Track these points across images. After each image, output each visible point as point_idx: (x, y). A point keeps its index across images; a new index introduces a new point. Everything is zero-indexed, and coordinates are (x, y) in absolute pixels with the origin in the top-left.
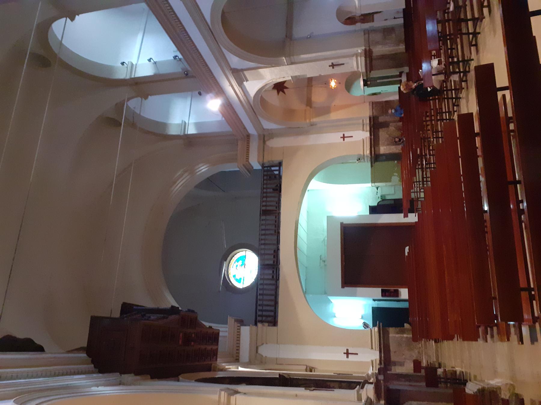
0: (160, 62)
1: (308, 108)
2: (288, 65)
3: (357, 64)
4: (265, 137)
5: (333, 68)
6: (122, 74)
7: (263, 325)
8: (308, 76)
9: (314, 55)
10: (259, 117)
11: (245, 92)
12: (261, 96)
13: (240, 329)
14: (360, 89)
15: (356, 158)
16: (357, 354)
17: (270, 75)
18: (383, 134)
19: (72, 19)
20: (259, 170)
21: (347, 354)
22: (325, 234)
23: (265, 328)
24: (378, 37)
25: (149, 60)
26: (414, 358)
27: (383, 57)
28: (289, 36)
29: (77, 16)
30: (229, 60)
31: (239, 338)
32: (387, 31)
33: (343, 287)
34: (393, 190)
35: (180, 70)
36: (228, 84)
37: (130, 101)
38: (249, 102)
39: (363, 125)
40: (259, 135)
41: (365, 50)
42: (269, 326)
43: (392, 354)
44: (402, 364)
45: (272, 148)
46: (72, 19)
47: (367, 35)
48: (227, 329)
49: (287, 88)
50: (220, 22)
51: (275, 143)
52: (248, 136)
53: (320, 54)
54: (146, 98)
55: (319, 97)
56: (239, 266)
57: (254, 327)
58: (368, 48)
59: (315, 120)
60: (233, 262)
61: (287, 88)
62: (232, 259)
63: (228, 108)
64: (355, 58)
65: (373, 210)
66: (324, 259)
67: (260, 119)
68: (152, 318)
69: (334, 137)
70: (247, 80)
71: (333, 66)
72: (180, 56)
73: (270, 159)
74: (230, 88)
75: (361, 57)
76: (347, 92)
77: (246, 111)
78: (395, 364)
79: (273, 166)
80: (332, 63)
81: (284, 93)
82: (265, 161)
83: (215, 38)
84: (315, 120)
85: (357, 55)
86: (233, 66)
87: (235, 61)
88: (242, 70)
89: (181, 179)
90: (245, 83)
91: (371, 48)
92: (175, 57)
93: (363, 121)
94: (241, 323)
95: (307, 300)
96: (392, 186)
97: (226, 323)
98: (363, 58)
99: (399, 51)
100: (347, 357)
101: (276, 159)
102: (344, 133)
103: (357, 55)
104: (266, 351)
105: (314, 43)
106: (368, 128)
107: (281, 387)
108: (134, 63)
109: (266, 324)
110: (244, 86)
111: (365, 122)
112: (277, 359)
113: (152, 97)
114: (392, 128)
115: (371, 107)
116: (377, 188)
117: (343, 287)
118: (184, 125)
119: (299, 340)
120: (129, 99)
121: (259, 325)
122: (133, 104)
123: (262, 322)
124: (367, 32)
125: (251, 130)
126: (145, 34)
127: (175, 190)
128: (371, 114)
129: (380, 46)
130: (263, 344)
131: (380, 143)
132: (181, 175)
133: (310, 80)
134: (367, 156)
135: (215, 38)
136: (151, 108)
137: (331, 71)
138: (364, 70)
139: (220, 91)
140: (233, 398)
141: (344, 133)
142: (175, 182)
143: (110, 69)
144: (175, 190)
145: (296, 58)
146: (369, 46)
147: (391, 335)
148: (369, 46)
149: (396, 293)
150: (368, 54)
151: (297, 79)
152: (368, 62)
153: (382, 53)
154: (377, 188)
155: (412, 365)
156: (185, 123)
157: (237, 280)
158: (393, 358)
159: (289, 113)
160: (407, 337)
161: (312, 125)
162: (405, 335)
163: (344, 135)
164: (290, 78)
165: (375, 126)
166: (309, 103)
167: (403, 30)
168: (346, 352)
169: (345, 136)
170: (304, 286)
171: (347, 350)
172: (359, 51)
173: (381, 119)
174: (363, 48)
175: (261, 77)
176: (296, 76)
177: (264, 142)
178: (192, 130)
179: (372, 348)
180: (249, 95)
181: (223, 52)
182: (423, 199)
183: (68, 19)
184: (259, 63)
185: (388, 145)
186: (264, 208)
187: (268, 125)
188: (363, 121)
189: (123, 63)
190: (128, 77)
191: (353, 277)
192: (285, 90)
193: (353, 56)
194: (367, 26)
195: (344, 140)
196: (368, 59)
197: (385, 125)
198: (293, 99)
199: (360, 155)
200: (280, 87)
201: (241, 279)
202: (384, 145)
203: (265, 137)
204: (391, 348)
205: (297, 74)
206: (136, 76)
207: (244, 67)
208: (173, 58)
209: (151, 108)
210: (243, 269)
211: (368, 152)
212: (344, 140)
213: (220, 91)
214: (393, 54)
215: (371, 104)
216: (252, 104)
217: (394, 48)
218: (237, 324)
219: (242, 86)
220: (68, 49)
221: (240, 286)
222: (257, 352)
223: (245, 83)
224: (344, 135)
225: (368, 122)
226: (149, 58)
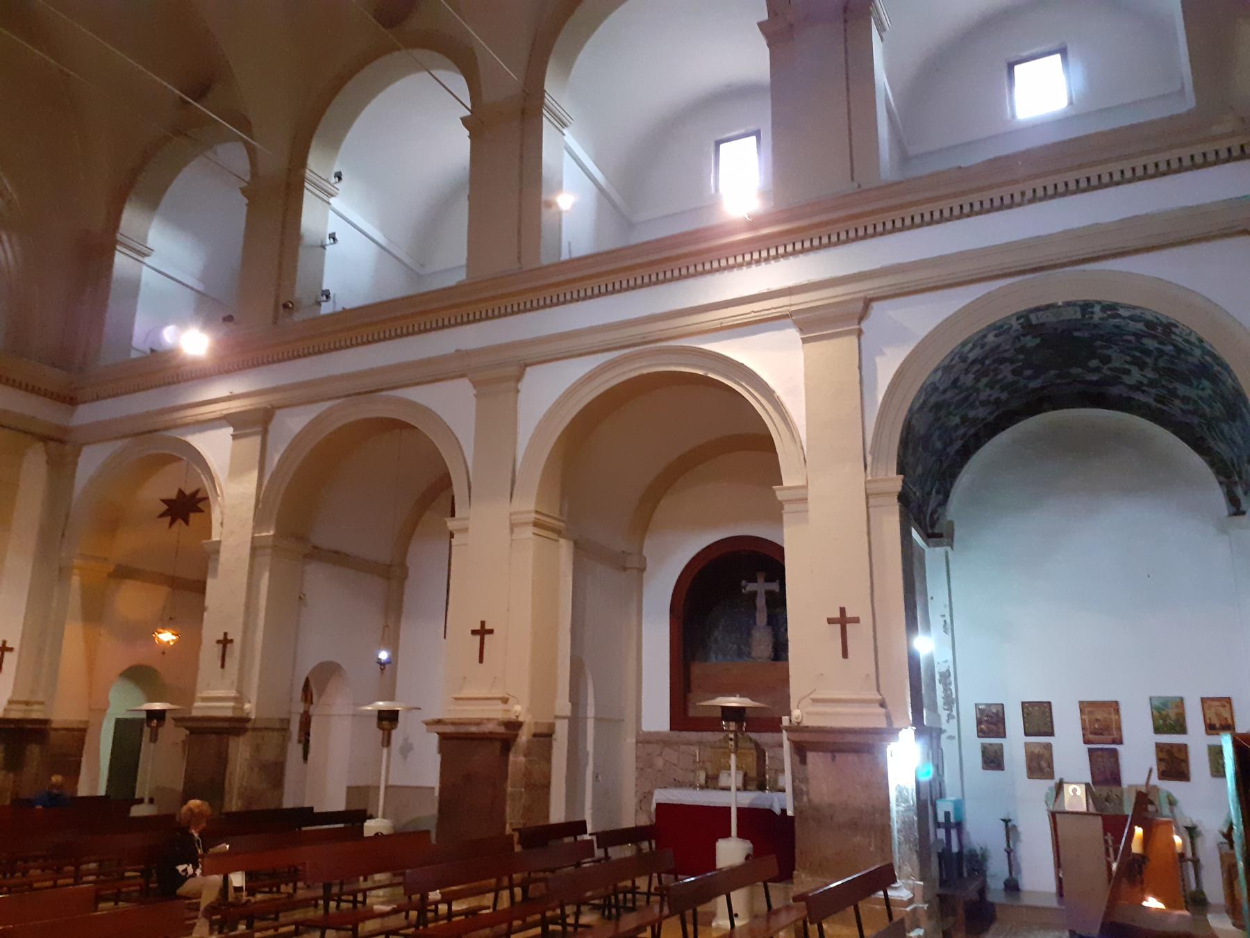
0: (323, 255)
1: (111, 568)
2: (253, 538)
3: (215, 695)
5: (218, 642)
6: (315, 164)
8: (210, 583)
9: (263, 602)
10: (126, 441)
12: (180, 459)
14: (126, 702)
24: (269, 755)
25: (333, 236)
27: (222, 760)
28: (316, 554)
32: (275, 773)
35: (298, 293)
37: (245, 152)
38: (176, 427)
39: (27, 703)
40: (66, 430)
41: (248, 720)
47: (278, 726)
49: (171, 523)
50: (395, 417)
52: (71, 400)
53: (262, 614)
55: (132, 601)
58: (249, 725)
59: (76, 580)
61: (171, 523)
63: (162, 370)
64: (233, 693)
67: (119, 444)
70: (235, 437)
71: (225, 642)
72: (326, 308)
74: (228, 393)
75: (234, 708)
76: (125, 667)
77: (149, 415)
80: (231, 641)
83: (359, 394)
84: (76, 580)
85: (239, 699)
86: (278, 413)
87: (293, 423)
88: (264, 434)
91: (249, 734)
92: (327, 294)
93: (42, 703)
98: (229, 714)
99: (227, 799)
103: (239, 699)
105: (289, 605)
106: (15, 715)
108: (332, 200)
110: (221, 427)
111: (36, 707)
113: (245, 209)
115: (75, 726)
118: (142, 253)
120: (251, 151)
122: (234, 156)
124: (283, 727)
125: (86, 414)
128: (54, 726)
129: (248, 755)
133: (200, 588)
135: (359, 394)
137: (211, 632)
138: (195, 713)
139: (220, 369)
143: (334, 144)
145: (265, 559)
146: (254, 729)
148: (254, 729)
150: (237, 726)
151: (207, 557)
152: (220, 724)
153: (231, 755)
156: (145, 255)
159: (112, 521)
161: (60, 569)
164: (215, 538)
166: (123, 573)
167: (272, 806)
172: (247, 706)
173: (34, 750)
175: (236, 470)
176: (218, 552)
177: (45, 439)
178: (122, 261)
180: (194, 433)
182: (653, 843)
184: (274, 475)
188: (42, 703)
189: (339, 176)
190: (308, 174)
192: (168, 519)
193: (239, 691)
194: (295, 728)
196: (226, 725)
198: (148, 538)
200: (188, 506)
203: (60, 447)
205: (224, 556)
206: (306, 191)
208: (324, 288)
213: (220, 369)
215: (82, 726)
216: (167, 433)
217: (236, 785)
219: (224, 422)
220: (404, 75)
223: (230, 430)
225: (34, 716)
226: (337, 236)
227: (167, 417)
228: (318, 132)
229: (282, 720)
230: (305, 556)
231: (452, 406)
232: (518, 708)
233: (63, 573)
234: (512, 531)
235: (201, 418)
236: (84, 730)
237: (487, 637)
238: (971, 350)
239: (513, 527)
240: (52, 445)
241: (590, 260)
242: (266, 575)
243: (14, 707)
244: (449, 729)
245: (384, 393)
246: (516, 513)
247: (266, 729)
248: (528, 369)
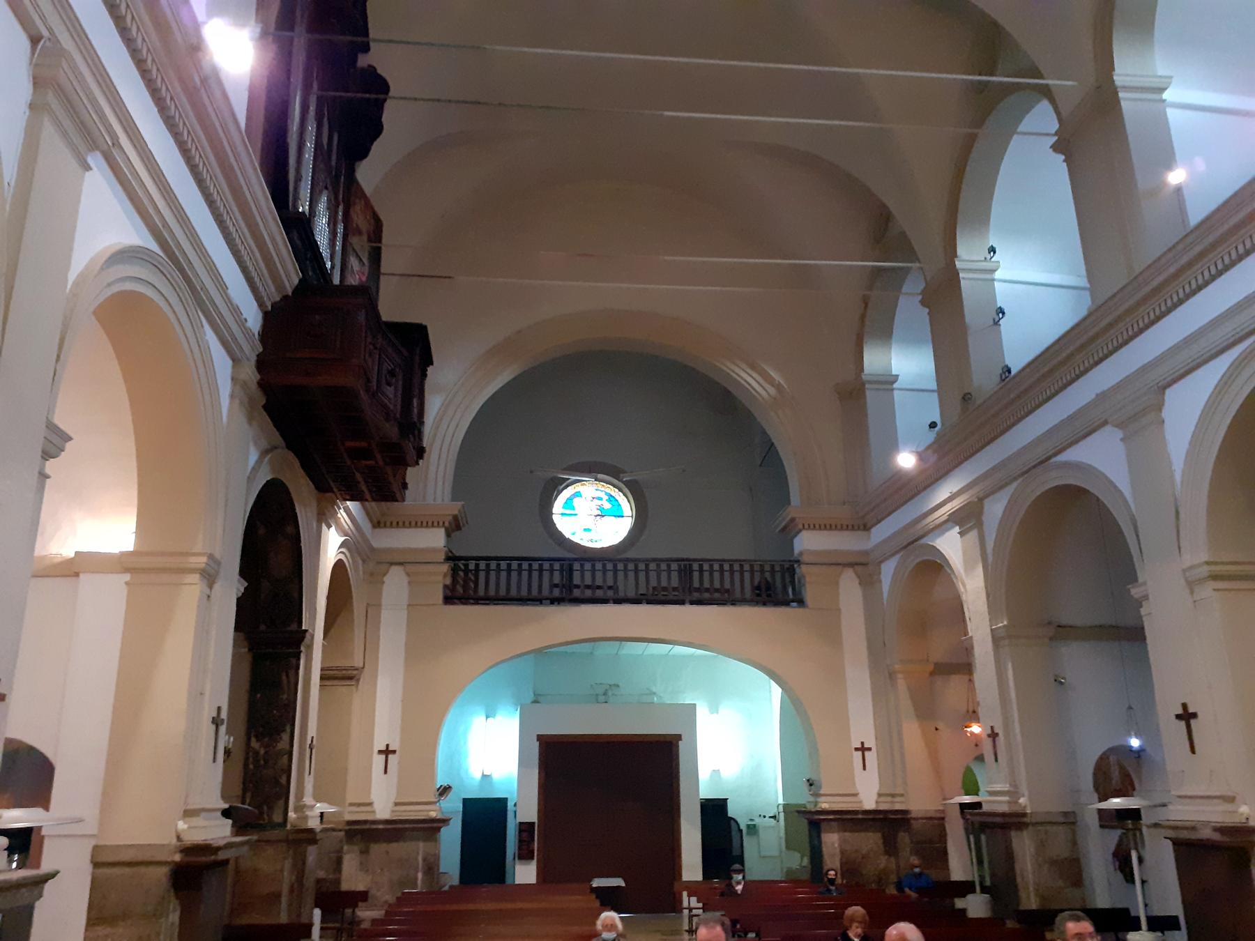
1: (931, 667)
4: (864, 566)
7: (445, 576)
11: (941, 527)
13: (438, 526)
15: (814, 777)
16: (386, 772)
17: (972, 586)
18: (869, 841)
19: (1056, 148)
20: (793, 549)
21: (387, 752)
22: (668, 700)
23: (440, 578)
24: (1059, 849)
26: (373, 892)
27: (1010, 856)
28: (1063, 632)
29: (1063, 157)
30: (997, 495)
31: (422, 526)
33: (540, 738)
34: (768, 857)
36: (955, 490)
39: (893, 796)
41: (1024, 815)
42: (445, 587)
43: (383, 847)
44: (364, 867)
45: (837, 583)
46: (1056, 148)
47: (1062, 819)
48: (439, 501)
51: (849, 590)
52: (866, 528)
54: (923, 303)
55: (1083, 664)
56: (599, 502)
57: (442, 557)
58: (1026, 820)
60: (608, 491)
62: (614, 486)
63: (909, 489)
64: (1006, 787)
65: (714, 811)
66: (610, 693)
68: (390, 391)
69: (863, 728)
73: (807, 579)
74: (948, 494)
75: (1009, 802)
78: (365, 852)
79: (794, 589)
81: (52, 876)
82: (804, 567)
84: (901, 683)
87: (995, 509)
88: (979, 525)
89: (762, 381)
90: (957, 529)
91: (1030, 828)
93: (902, 795)
94: (454, 527)
95: (497, 664)
96: (781, 852)
97: (453, 499)
98: (1004, 808)
99: (1023, 895)
100: (380, 752)
101: (809, 594)
102: (874, 749)
103: (1014, 794)
104: (396, 584)
106: (883, 807)
107: (1237, 187)
109: (448, 581)
111: (898, 799)
112: (380, 605)
114: (883, 861)
115: (933, 815)
116: (774, 817)
117: (540, 738)
119: (418, 651)
121: (445, 568)
123: (455, 571)
126: (1075, 292)
127: (737, 370)
128: (913, 815)
130: (408, 574)
131: (847, 834)
132: (771, 381)
134: (816, 803)
136: (910, 309)
140: (195, 578)
141: (874, 749)
142: (753, 367)
143: (982, 220)
144: (737, 370)
147: (421, 844)
149: (525, 854)
150: (1013, 821)
154: (774, 817)
155: (361, 887)
157: (570, 499)
158: (377, 849)
160: (416, 879)
161: (890, 675)
162: (420, 875)
163: (869, 749)
165: (888, 822)
168: (391, 748)
169: (867, 753)
170: (562, 649)
171: (394, 752)
173: (904, 838)
174: (1028, 811)
175: (969, 566)
177: (851, 565)
179: (396, 804)
181: (1007, 484)
183: (1056, 138)
185: (842, 852)
186: (696, 566)
187: (888, 570)
188: (902, 795)
191: (558, 759)
195: (857, 749)
197: (890, 847)
199: (820, 787)
201: (573, 509)
202: (843, 841)
204: (394, 845)
207: (985, 527)
209: (910, 309)
210: (592, 516)
211: (825, 806)
212: (857, 749)
214: (1015, 879)
215: (938, 815)
216: (923, 541)
218: (448, 520)
221: (558, 506)
222: (392, 564)
223: (957, 529)
224: (869, 749)
225: (898, 807)
227: (919, 526)
228: (960, 217)
229: (1065, 814)
230: (1051, 639)
231: (1104, 457)
232: (1244, 809)
233: (892, 676)
234: (1192, 592)
235: (938, 522)
236: (943, 819)
237: (1193, 722)
238: (669, 578)
239: (1192, 585)
240: (859, 568)
241: (1170, 255)
242: (1010, 666)
243: (882, 799)
244: (1185, 835)
245: (1054, 460)
246: (1191, 568)
247: (1050, 823)
248: (1168, 391)
